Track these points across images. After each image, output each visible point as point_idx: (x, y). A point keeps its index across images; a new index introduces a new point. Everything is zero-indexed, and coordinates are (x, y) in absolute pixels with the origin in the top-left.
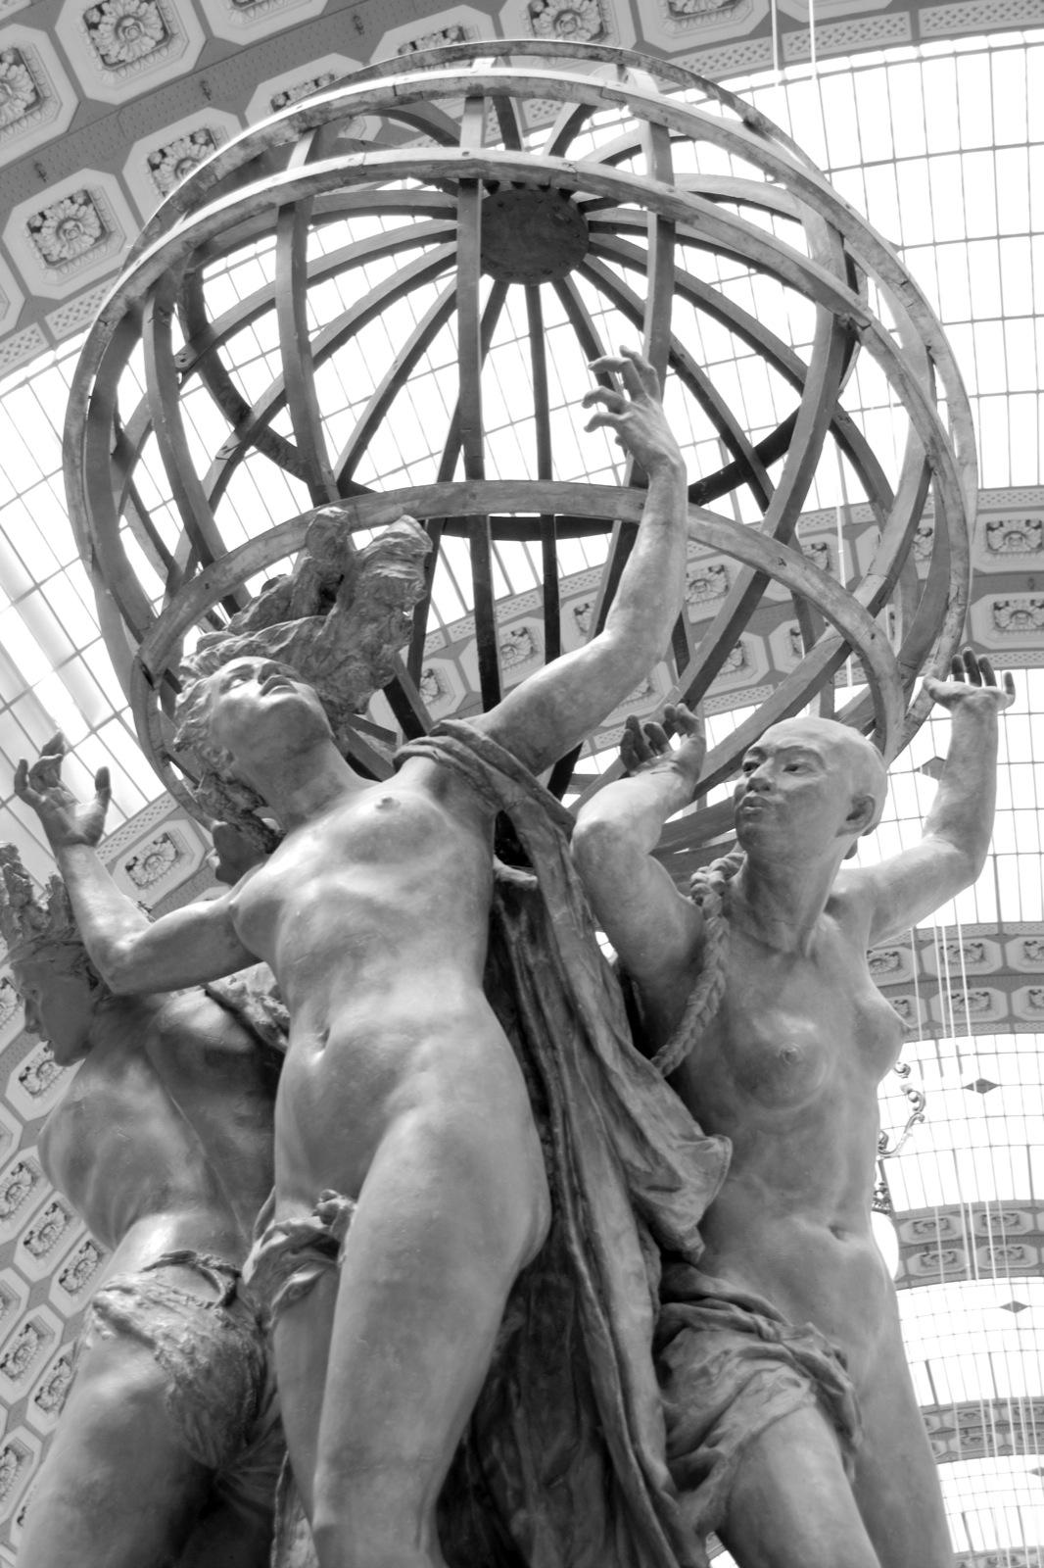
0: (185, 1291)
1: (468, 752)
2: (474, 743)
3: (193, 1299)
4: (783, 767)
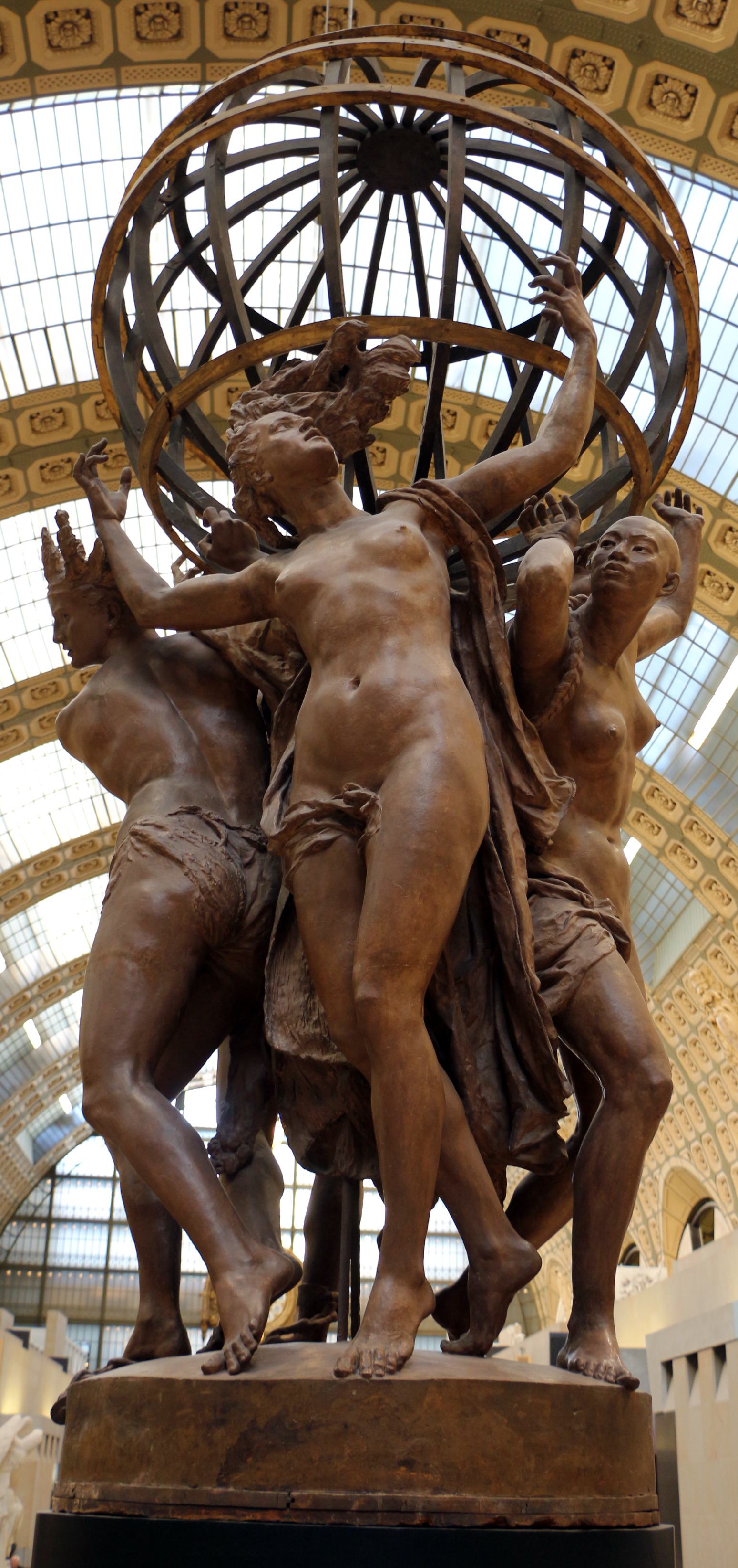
0: (199, 832)
1: (442, 503)
2: (447, 497)
3: (206, 838)
4: (633, 547)
